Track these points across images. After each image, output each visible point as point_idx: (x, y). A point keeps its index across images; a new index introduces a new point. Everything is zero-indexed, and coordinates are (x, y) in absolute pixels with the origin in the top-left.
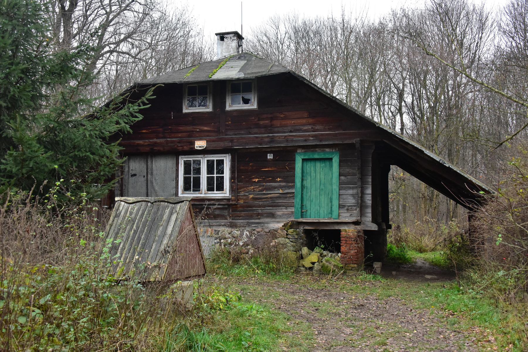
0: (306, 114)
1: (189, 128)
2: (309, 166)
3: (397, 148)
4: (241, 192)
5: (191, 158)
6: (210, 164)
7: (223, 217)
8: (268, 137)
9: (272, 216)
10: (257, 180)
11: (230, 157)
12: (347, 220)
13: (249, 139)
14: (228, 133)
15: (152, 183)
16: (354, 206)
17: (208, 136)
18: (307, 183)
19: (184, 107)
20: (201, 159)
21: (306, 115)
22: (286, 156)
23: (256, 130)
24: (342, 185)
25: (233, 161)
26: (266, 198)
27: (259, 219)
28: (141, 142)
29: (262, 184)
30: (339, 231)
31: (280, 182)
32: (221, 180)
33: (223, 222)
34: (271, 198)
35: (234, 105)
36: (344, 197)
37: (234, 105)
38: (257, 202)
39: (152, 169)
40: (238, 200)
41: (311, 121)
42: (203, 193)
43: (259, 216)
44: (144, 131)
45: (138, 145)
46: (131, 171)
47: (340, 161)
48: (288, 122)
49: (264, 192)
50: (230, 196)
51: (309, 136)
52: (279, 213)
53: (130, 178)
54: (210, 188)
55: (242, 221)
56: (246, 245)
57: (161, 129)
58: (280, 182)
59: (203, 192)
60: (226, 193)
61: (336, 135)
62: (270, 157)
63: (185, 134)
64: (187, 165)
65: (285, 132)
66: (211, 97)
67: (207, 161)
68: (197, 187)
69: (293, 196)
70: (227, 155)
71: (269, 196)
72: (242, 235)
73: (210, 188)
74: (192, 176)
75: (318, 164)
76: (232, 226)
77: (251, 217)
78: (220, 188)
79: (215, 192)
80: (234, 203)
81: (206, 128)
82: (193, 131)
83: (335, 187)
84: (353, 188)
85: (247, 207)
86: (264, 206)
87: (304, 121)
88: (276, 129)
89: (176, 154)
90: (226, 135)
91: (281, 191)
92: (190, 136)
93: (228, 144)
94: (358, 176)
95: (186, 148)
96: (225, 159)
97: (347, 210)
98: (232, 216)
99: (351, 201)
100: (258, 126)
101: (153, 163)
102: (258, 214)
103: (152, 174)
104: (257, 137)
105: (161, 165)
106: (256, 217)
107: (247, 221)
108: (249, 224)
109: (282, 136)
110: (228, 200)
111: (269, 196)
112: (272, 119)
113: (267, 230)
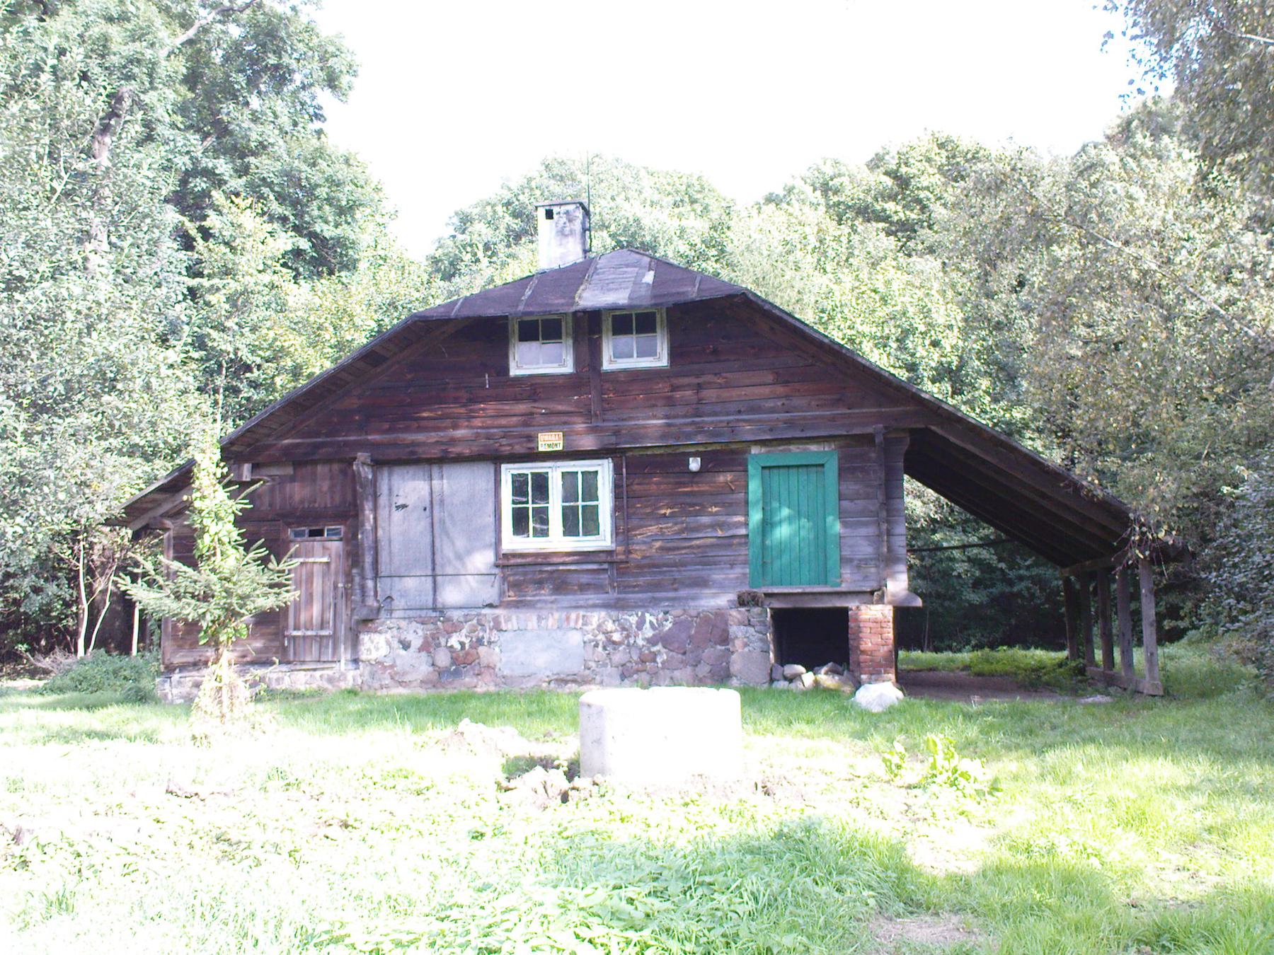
2: (777, 478)
5: (528, 469)
7: (598, 588)
9: (703, 583)
10: (669, 511)
11: (611, 465)
13: (651, 425)
14: (606, 417)
19: (512, 365)
21: (770, 378)
25: (617, 470)
27: (676, 590)
29: (679, 520)
30: (845, 611)
33: (593, 598)
34: (699, 547)
35: (619, 356)
37: (619, 356)
41: (780, 390)
44: (425, 415)
45: (413, 444)
46: (395, 499)
48: (735, 393)
49: (684, 535)
55: (640, 595)
56: (652, 641)
57: (462, 410)
60: (603, 540)
61: (833, 419)
63: (515, 419)
65: (728, 414)
66: (570, 342)
69: (746, 544)
71: (698, 542)
77: (656, 586)
78: (592, 527)
80: (623, 557)
82: (532, 414)
84: (865, 524)
87: (766, 390)
88: (707, 409)
94: (881, 497)
95: (519, 449)
107: (650, 594)
110: (610, 553)
111: (698, 542)
112: (699, 387)
113: (694, 613)
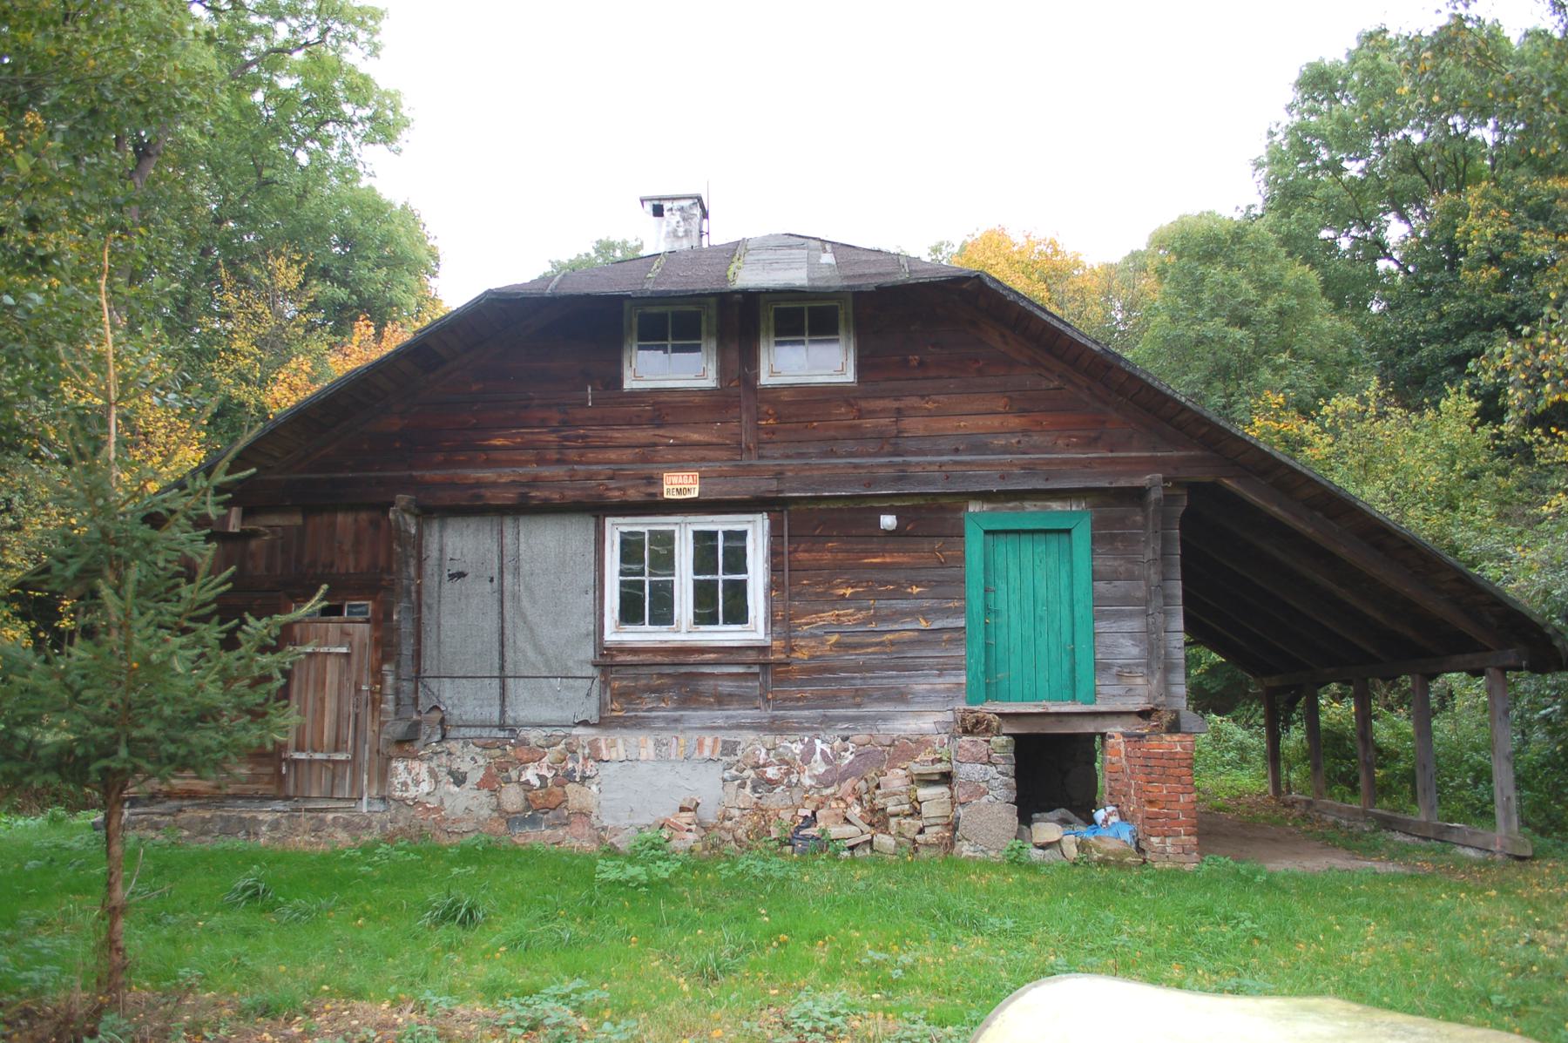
0: (1002, 402)
1: (643, 435)
2: (1003, 547)
3: (1252, 497)
4: (800, 625)
6: (704, 541)
8: (891, 465)
9: (901, 697)
10: (849, 591)
11: (767, 522)
12: (1118, 706)
14: (765, 452)
15: (516, 598)
16: (1138, 665)
17: (703, 459)
18: (1001, 600)
20: (676, 528)
21: (1000, 404)
22: (932, 518)
23: (851, 446)
24: (1102, 607)
25: (775, 533)
26: (877, 644)
27: (858, 706)
28: (488, 475)
29: (865, 604)
31: (918, 597)
32: (738, 591)
33: (746, 714)
34: (892, 643)
35: (791, 365)
36: (1108, 640)
38: (851, 657)
39: (517, 558)
40: (792, 650)
41: (1014, 422)
42: (684, 630)
43: (861, 696)
45: (479, 484)
47: (1095, 540)
49: (872, 627)
50: (769, 639)
51: (1011, 464)
52: (920, 687)
53: (447, 585)
54: (705, 616)
55: (806, 713)
58: (918, 597)
59: (684, 629)
60: (755, 630)
62: (888, 521)
64: (631, 548)
66: (714, 344)
67: (697, 534)
68: (663, 614)
70: (758, 517)
72: (807, 756)
73: (705, 616)
74: (647, 579)
75: (1026, 543)
76: (777, 727)
77: (831, 700)
78: (737, 614)
79: (647, 627)
81: (696, 437)
82: (656, 445)
83: (1084, 608)
85: (819, 671)
86: (871, 669)
89: (598, 509)
90: (761, 457)
91: (923, 625)
92: (645, 460)
93: (767, 486)
95: (634, 495)
96: (676, 528)
97: (1119, 675)
98: (774, 699)
99: (1129, 650)
100: (858, 435)
101: (522, 540)
102: (857, 692)
103: (517, 571)
104: (856, 466)
105: (548, 544)
106: (850, 701)
108: (828, 722)
109: (930, 463)
110: (763, 650)
111: (889, 637)
